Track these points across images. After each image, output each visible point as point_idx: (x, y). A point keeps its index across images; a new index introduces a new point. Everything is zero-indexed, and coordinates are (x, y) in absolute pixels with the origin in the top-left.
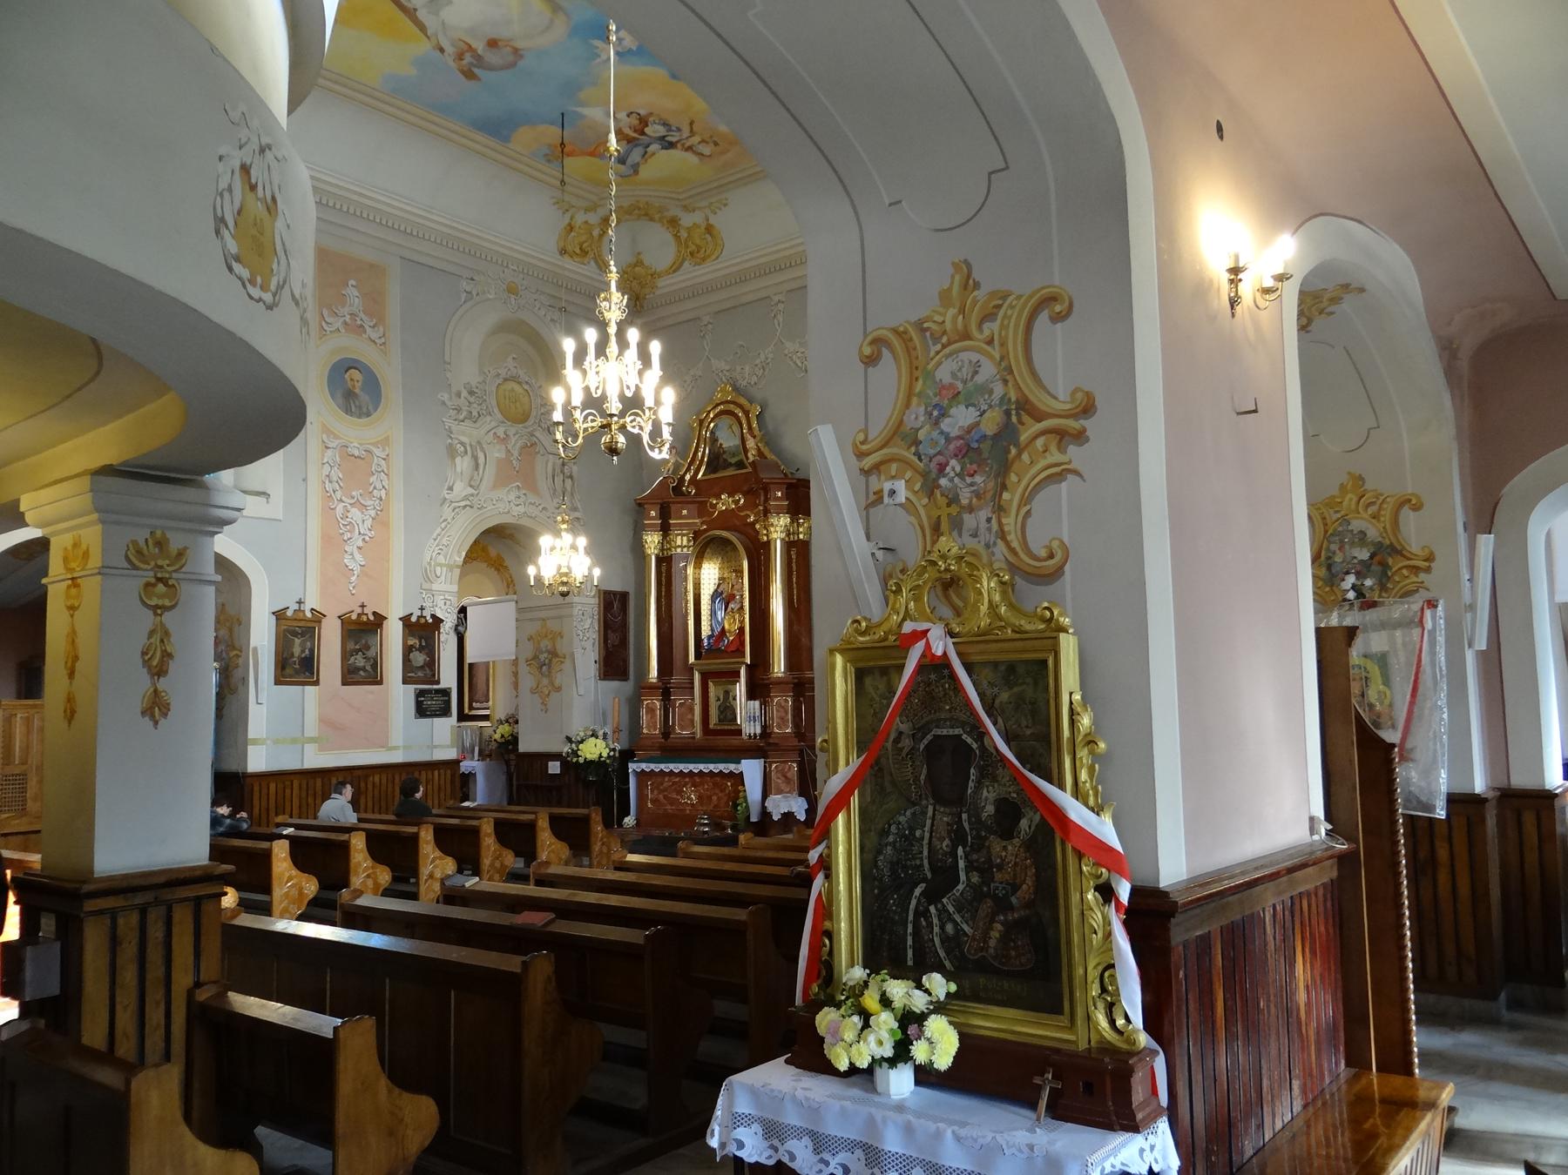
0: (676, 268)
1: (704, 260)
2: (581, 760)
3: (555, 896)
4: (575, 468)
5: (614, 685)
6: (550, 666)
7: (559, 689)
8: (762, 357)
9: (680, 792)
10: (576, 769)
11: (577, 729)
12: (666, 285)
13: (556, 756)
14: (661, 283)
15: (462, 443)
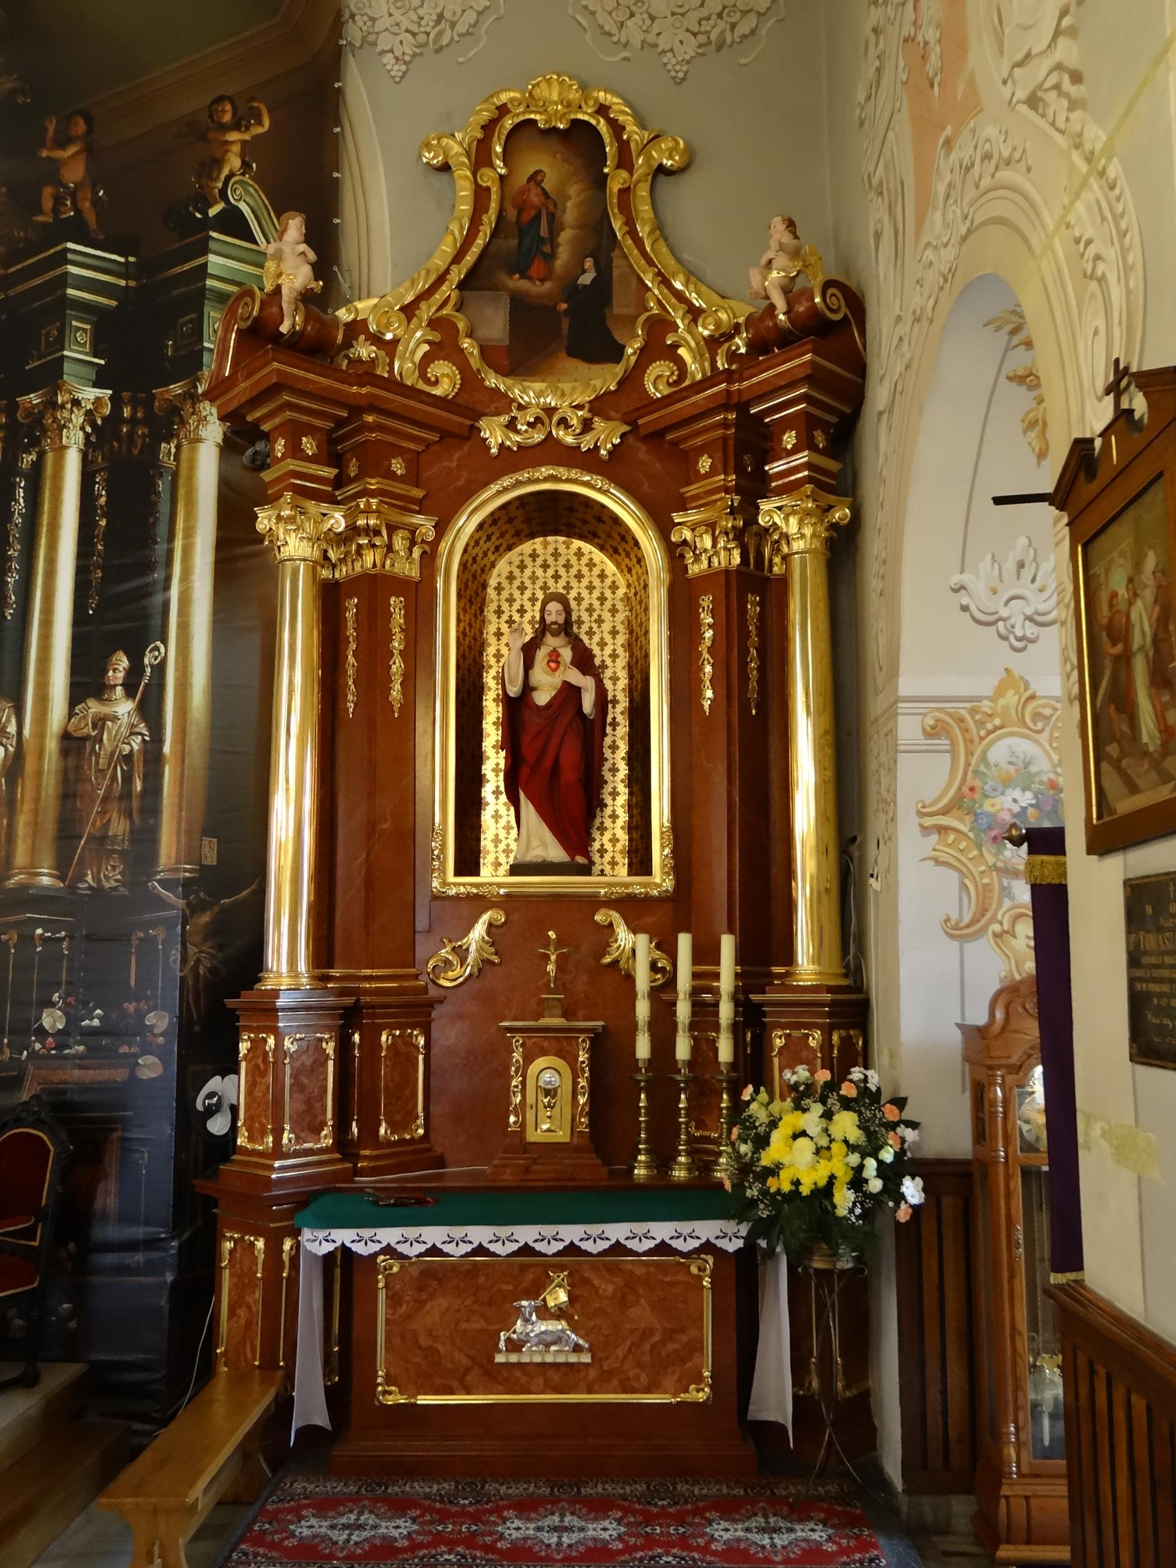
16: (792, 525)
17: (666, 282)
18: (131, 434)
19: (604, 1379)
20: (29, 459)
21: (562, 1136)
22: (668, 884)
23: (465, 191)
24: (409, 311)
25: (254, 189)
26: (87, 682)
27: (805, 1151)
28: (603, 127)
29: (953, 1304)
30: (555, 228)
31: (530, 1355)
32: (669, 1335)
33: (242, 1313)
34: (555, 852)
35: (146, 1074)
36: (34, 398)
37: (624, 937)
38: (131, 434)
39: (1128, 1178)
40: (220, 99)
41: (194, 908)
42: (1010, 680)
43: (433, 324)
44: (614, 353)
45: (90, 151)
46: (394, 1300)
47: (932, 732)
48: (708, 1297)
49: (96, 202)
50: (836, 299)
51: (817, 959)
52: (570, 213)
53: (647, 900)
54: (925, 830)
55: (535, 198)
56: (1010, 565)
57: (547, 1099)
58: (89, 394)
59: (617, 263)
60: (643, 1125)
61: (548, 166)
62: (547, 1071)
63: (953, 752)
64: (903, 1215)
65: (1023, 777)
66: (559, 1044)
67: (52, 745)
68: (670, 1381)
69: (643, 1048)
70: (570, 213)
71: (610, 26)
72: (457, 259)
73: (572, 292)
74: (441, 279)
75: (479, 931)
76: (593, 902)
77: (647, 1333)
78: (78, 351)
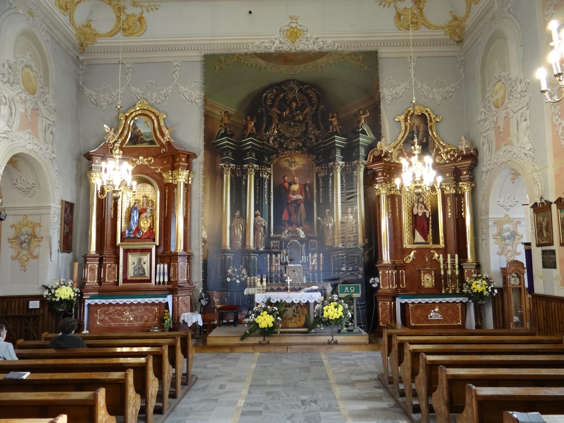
0: (111, 34)
1: (131, 34)
2: (58, 300)
3: (542, 394)
4: (54, 129)
5: (65, 255)
6: (29, 243)
7: (36, 257)
8: (165, 91)
9: (121, 315)
10: (50, 304)
11: (50, 279)
12: (102, 42)
13: (34, 298)
14: (99, 40)
15: (5, 97)
16: (466, 188)
17: (439, 143)
18: (349, 170)
19: (445, 321)
20: (331, 174)
21: (431, 286)
22: (444, 246)
23: (403, 126)
24: (395, 147)
25: (367, 126)
26: (344, 213)
27: (478, 286)
28: (427, 115)
29: (500, 308)
31: (433, 318)
32: (454, 315)
33: (384, 314)
34: (423, 241)
35: (360, 278)
36: (331, 164)
37: (436, 255)
38: (349, 170)
39: (542, 281)
40: (360, 110)
41: (365, 250)
42: (506, 215)
43: (399, 150)
45: (338, 119)
46: (412, 310)
47: (495, 223)
48: (460, 310)
49: (340, 129)
50: (475, 152)
51: (471, 258)
54: (494, 239)
56: (507, 198)
57: (428, 281)
58: (341, 163)
61: (417, 122)
62: (427, 276)
63: (498, 226)
64: (494, 295)
65: (508, 230)
66: (429, 272)
67: (339, 224)
68: (455, 322)
69: (442, 273)
71: (426, 95)
75: (412, 253)
77: (451, 315)
78: (338, 155)
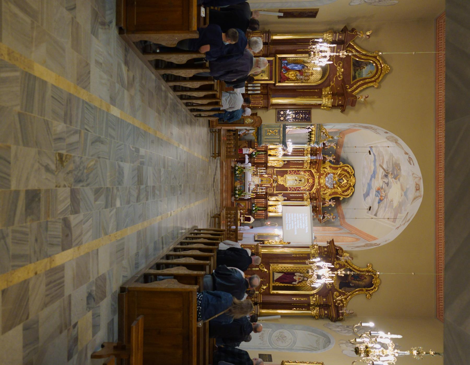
16: (314, 312)
28: (372, 288)
30: (358, 281)
34: (275, 278)
44: (340, 288)
52: (361, 283)
53: (269, 290)
55: (363, 278)
59: (353, 289)
60: (407, 353)
61: (367, 280)
70: (361, 283)
72: (354, 268)
73: (349, 283)
74: (351, 267)
75: (266, 270)
76: (269, 283)
